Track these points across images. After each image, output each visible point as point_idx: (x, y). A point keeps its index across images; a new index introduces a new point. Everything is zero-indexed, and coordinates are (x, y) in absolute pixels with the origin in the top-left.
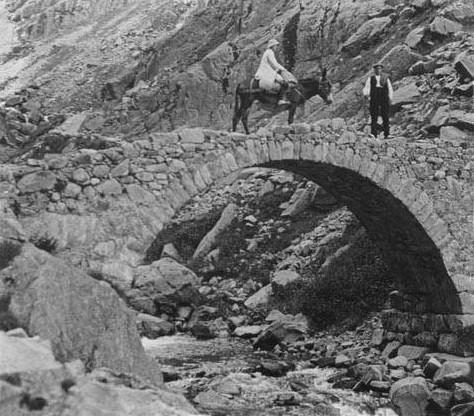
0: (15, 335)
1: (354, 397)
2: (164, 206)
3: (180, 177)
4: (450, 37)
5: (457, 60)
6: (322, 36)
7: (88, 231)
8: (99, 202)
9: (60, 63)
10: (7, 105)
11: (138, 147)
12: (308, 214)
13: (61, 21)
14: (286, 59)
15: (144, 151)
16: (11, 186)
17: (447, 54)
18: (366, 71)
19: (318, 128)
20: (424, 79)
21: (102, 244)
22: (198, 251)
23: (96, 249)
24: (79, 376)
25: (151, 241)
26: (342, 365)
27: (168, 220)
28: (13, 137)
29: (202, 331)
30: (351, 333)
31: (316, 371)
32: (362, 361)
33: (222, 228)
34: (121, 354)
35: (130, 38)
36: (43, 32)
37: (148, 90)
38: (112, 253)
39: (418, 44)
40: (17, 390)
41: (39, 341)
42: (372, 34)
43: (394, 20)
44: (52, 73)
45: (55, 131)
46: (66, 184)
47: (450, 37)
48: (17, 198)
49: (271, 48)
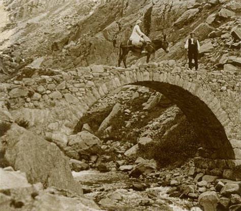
1: (180, 201)
2: (83, 104)
3: (91, 90)
4: (229, 19)
5: (232, 31)
6: (164, 18)
8: (50, 103)
9: (30, 32)
10: (3, 53)
11: (70, 75)
13: (31, 11)
14: (145, 30)
15: (73, 77)
16: (6, 95)
17: (227, 27)
18: (186, 36)
20: (216, 40)
23: (49, 126)
25: (77, 123)
26: (174, 185)
27: (85, 111)
28: (6, 70)
30: (179, 169)
31: (161, 188)
32: (184, 183)
33: (113, 116)
36: (22, 16)
37: (75, 45)
38: (57, 128)
39: (213, 22)
40: (9, 198)
41: (20, 173)
42: (189, 17)
43: (200, 10)
44: (26, 37)
45: (28, 66)
46: (34, 93)
47: (229, 19)
48: (9, 101)
49: (138, 24)
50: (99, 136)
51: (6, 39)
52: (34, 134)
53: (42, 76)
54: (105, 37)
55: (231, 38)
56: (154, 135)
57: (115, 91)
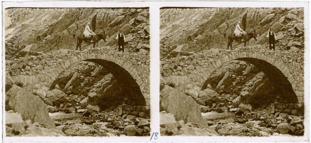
0: (10, 112)
1: (113, 131)
2: (207, 73)
3: (60, 64)
4: (293, 19)
5: (144, 29)
6: (104, 21)
7: (32, 81)
8: (36, 72)
9: (175, 30)
10: (8, 42)
11: (47, 55)
12: (99, 75)
13: (24, 17)
14: (93, 28)
15: (49, 56)
16: (9, 67)
17: (142, 27)
18: (117, 32)
19: (102, 49)
20: (135, 34)
21: (189, 84)
22: (66, 87)
23: (35, 86)
24: (30, 125)
25: (52, 84)
26: (110, 121)
27: (57, 77)
28: (10, 52)
29: (67, 111)
30: (112, 111)
31: (102, 123)
32: (116, 120)
33: (73, 80)
34: (43, 118)
35: (196, 22)
36: (19, 20)
37: (51, 38)
38: (40, 87)
39: (133, 24)
40: (11, 129)
41: (17, 114)
42: (119, 21)
43: (126, 16)
44: (21, 32)
45: (23, 50)
46: (26, 66)
47: (293, 19)
48: (11, 71)
49: (88, 25)
50: (65, 91)
51: (9, 34)
52: (26, 90)
53: (182, 56)
54: (68, 32)
55: (294, 31)
56: (249, 90)
57: (75, 65)
